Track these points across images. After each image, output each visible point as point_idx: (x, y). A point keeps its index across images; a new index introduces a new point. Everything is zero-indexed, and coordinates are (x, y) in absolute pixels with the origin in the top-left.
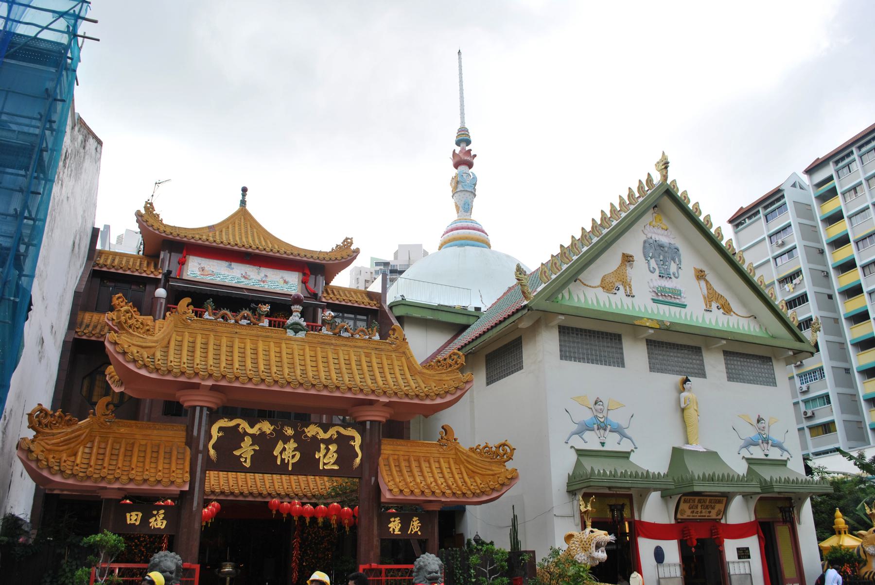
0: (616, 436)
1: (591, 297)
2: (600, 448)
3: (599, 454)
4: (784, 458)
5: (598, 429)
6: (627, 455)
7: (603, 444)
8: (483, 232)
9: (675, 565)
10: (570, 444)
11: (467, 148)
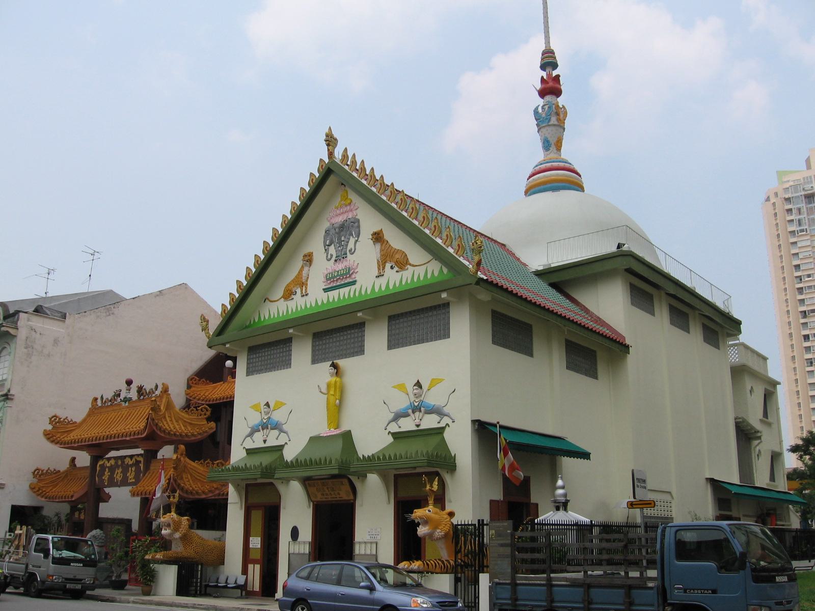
0: (276, 432)
1: (277, 309)
2: (263, 445)
3: (256, 451)
4: (442, 425)
5: (413, 412)
6: (441, 431)
7: (265, 441)
8: (570, 164)
9: (304, 542)
10: (243, 446)
11: (555, 73)
